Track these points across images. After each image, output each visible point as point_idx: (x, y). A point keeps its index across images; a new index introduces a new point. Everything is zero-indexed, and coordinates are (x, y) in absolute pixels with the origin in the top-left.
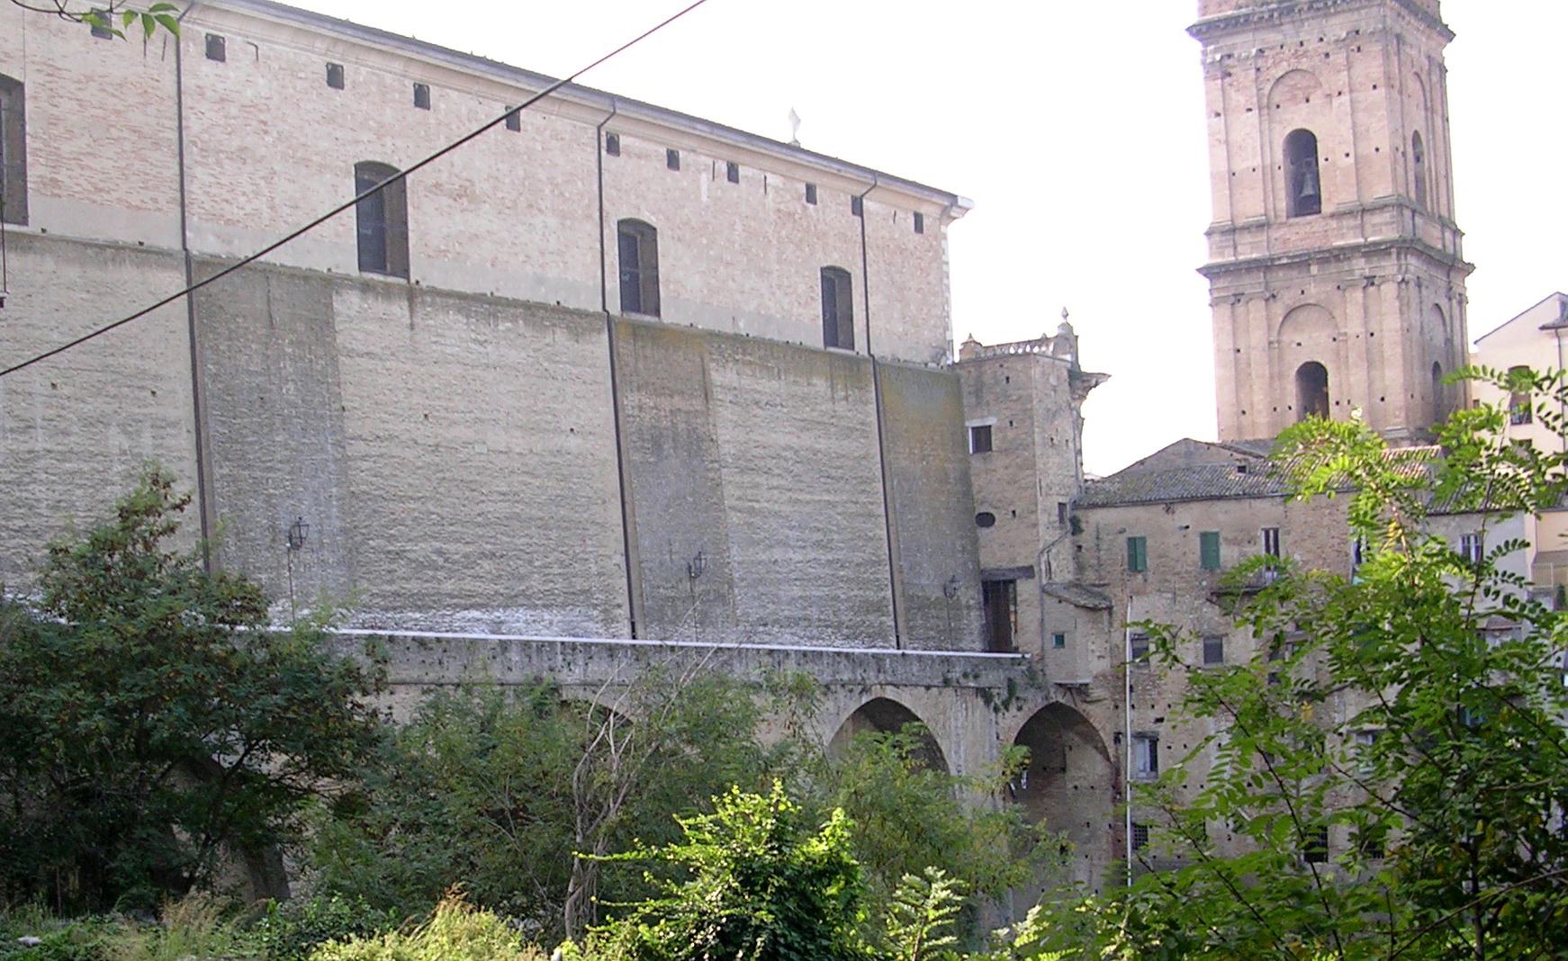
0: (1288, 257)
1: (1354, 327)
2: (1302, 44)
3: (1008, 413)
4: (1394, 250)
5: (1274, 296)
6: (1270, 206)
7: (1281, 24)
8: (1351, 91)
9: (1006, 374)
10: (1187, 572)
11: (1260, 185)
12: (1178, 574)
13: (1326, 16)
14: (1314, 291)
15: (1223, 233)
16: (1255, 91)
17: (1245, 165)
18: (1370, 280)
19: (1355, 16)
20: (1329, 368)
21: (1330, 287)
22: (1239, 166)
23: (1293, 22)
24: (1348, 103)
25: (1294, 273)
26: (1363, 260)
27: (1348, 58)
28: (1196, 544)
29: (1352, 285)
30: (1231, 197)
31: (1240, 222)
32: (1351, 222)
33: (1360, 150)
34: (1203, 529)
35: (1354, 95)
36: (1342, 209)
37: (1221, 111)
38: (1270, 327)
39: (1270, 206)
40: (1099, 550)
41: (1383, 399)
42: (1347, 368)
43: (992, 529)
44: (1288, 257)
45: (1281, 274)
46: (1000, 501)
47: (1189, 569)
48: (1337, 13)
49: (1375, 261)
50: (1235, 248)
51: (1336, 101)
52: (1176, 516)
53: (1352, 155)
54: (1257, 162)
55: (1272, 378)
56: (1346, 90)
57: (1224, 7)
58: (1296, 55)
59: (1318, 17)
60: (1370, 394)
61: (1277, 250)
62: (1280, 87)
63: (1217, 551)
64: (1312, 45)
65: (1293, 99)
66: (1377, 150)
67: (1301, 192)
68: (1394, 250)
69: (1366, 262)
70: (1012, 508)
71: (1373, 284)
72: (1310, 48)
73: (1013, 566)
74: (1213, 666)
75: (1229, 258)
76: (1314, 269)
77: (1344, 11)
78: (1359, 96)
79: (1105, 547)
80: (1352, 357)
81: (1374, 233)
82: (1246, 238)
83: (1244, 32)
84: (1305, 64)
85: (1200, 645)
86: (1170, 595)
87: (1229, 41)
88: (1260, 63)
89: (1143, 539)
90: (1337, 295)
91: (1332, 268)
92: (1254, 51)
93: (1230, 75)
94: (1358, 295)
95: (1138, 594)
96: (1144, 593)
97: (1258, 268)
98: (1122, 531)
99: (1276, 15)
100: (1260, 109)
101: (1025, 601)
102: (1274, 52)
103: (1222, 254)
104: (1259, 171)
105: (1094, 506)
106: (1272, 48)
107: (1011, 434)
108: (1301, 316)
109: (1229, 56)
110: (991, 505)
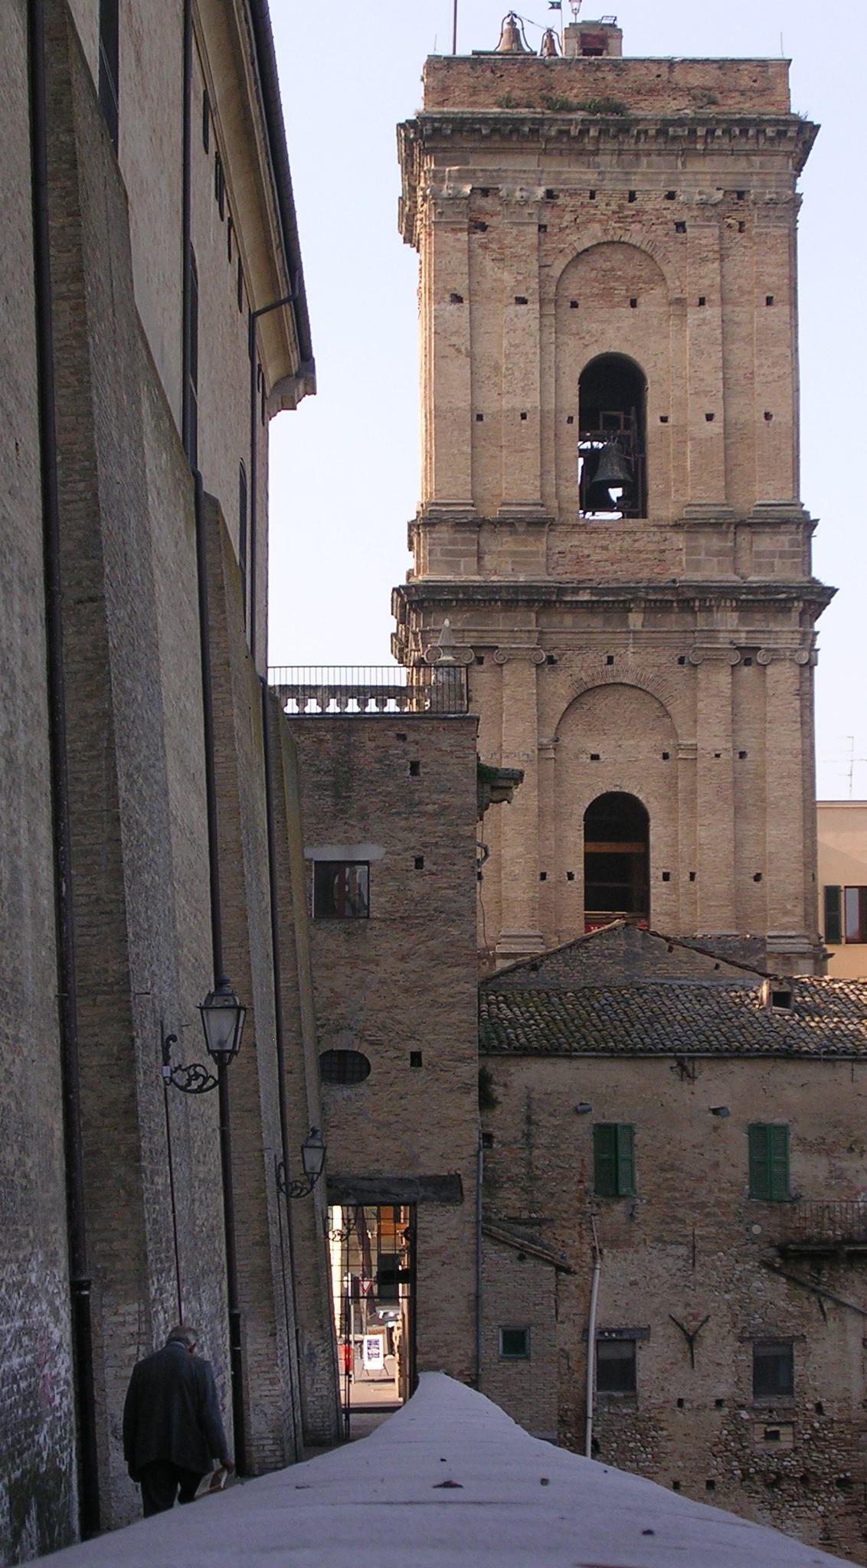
0: (594, 590)
1: (711, 737)
2: (632, 197)
3: (413, 839)
4: (799, 605)
5: (551, 660)
6: (550, 489)
7: (596, 153)
8: (724, 301)
9: (412, 757)
10: (718, 1203)
11: (533, 446)
12: (703, 1205)
13: (685, 153)
14: (632, 662)
15: (459, 526)
16: (535, 267)
17: (506, 403)
18: (747, 655)
19: (742, 165)
20: (653, 807)
21: (666, 657)
22: (497, 403)
23: (620, 153)
24: (717, 322)
25: (596, 623)
26: (735, 615)
27: (721, 237)
28: (738, 1149)
29: (713, 659)
30: (473, 458)
31: (493, 512)
32: (716, 543)
33: (733, 413)
34: (753, 1119)
35: (729, 308)
36: (699, 514)
37: (463, 292)
38: (541, 719)
39: (550, 489)
40: (531, 1147)
41: (757, 878)
42: (692, 811)
43: (362, 1088)
44: (594, 590)
45: (568, 620)
46: (383, 1028)
47: (725, 1197)
48: (705, 153)
49: (758, 622)
50: (480, 559)
51: (694, 315)
52: (699, 1086)
53: (719, 417)
54: (531, 401)
55: (541, 813)
56: (715, 297)
57: (483, 97)
58: (620, 216)
59: (670, 153)
60: (738, 864)
61: (564, 574)
62: (582, 270)
63: (785, 1164)
64: (652, 202)
65: (606, 295)
66: (768, 416)
67: (592, 477)
68: (799, 605)
69: (742, 621)
70: (413, 1046)
71: (748, 662)
72: (649, 207)
73: (408, 1173)
74: (774, 1401)
75: (466, 575)
76: (635, 620)
77: (720, 152)
78: (741, 314)
79: (544, 1140)
80: (705, 793)
81: (759, 568)
82: (506, 543)
83: (521, 151)
84: (636, 235)
85: (747, 1358)
86: (683, 1250)
87: (491, 164)
88: (547, 217)
89: (630, 1129)
90: (677, 676)
91: (672, 622)
92: (540, 192)
93: (484, 228)
94: (723, 678)
95: (615, 1244)
96: (629, 1244)
97: (530, 603)
98: (581, 1111)
99: (593, 133)
100: (542, 302)
101: (437, 1252)
102: (576, 201)
103: (453, 567)
104: (534, 419)
105: (525, 1052)
106: (573, 194)
107: (417, 886)
108: (601, 705)
109: (485, 192)
110: (360, 1036)
